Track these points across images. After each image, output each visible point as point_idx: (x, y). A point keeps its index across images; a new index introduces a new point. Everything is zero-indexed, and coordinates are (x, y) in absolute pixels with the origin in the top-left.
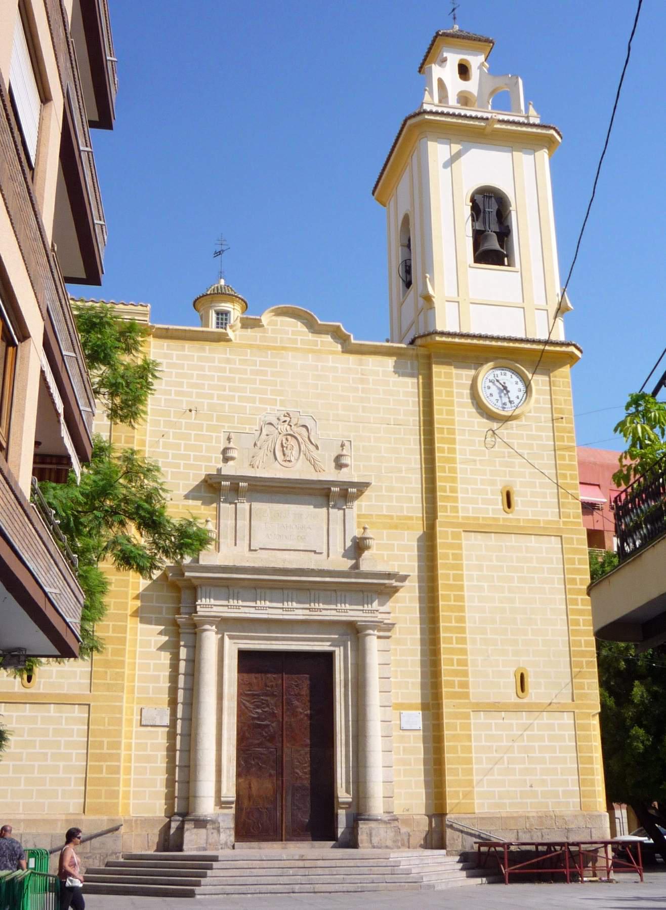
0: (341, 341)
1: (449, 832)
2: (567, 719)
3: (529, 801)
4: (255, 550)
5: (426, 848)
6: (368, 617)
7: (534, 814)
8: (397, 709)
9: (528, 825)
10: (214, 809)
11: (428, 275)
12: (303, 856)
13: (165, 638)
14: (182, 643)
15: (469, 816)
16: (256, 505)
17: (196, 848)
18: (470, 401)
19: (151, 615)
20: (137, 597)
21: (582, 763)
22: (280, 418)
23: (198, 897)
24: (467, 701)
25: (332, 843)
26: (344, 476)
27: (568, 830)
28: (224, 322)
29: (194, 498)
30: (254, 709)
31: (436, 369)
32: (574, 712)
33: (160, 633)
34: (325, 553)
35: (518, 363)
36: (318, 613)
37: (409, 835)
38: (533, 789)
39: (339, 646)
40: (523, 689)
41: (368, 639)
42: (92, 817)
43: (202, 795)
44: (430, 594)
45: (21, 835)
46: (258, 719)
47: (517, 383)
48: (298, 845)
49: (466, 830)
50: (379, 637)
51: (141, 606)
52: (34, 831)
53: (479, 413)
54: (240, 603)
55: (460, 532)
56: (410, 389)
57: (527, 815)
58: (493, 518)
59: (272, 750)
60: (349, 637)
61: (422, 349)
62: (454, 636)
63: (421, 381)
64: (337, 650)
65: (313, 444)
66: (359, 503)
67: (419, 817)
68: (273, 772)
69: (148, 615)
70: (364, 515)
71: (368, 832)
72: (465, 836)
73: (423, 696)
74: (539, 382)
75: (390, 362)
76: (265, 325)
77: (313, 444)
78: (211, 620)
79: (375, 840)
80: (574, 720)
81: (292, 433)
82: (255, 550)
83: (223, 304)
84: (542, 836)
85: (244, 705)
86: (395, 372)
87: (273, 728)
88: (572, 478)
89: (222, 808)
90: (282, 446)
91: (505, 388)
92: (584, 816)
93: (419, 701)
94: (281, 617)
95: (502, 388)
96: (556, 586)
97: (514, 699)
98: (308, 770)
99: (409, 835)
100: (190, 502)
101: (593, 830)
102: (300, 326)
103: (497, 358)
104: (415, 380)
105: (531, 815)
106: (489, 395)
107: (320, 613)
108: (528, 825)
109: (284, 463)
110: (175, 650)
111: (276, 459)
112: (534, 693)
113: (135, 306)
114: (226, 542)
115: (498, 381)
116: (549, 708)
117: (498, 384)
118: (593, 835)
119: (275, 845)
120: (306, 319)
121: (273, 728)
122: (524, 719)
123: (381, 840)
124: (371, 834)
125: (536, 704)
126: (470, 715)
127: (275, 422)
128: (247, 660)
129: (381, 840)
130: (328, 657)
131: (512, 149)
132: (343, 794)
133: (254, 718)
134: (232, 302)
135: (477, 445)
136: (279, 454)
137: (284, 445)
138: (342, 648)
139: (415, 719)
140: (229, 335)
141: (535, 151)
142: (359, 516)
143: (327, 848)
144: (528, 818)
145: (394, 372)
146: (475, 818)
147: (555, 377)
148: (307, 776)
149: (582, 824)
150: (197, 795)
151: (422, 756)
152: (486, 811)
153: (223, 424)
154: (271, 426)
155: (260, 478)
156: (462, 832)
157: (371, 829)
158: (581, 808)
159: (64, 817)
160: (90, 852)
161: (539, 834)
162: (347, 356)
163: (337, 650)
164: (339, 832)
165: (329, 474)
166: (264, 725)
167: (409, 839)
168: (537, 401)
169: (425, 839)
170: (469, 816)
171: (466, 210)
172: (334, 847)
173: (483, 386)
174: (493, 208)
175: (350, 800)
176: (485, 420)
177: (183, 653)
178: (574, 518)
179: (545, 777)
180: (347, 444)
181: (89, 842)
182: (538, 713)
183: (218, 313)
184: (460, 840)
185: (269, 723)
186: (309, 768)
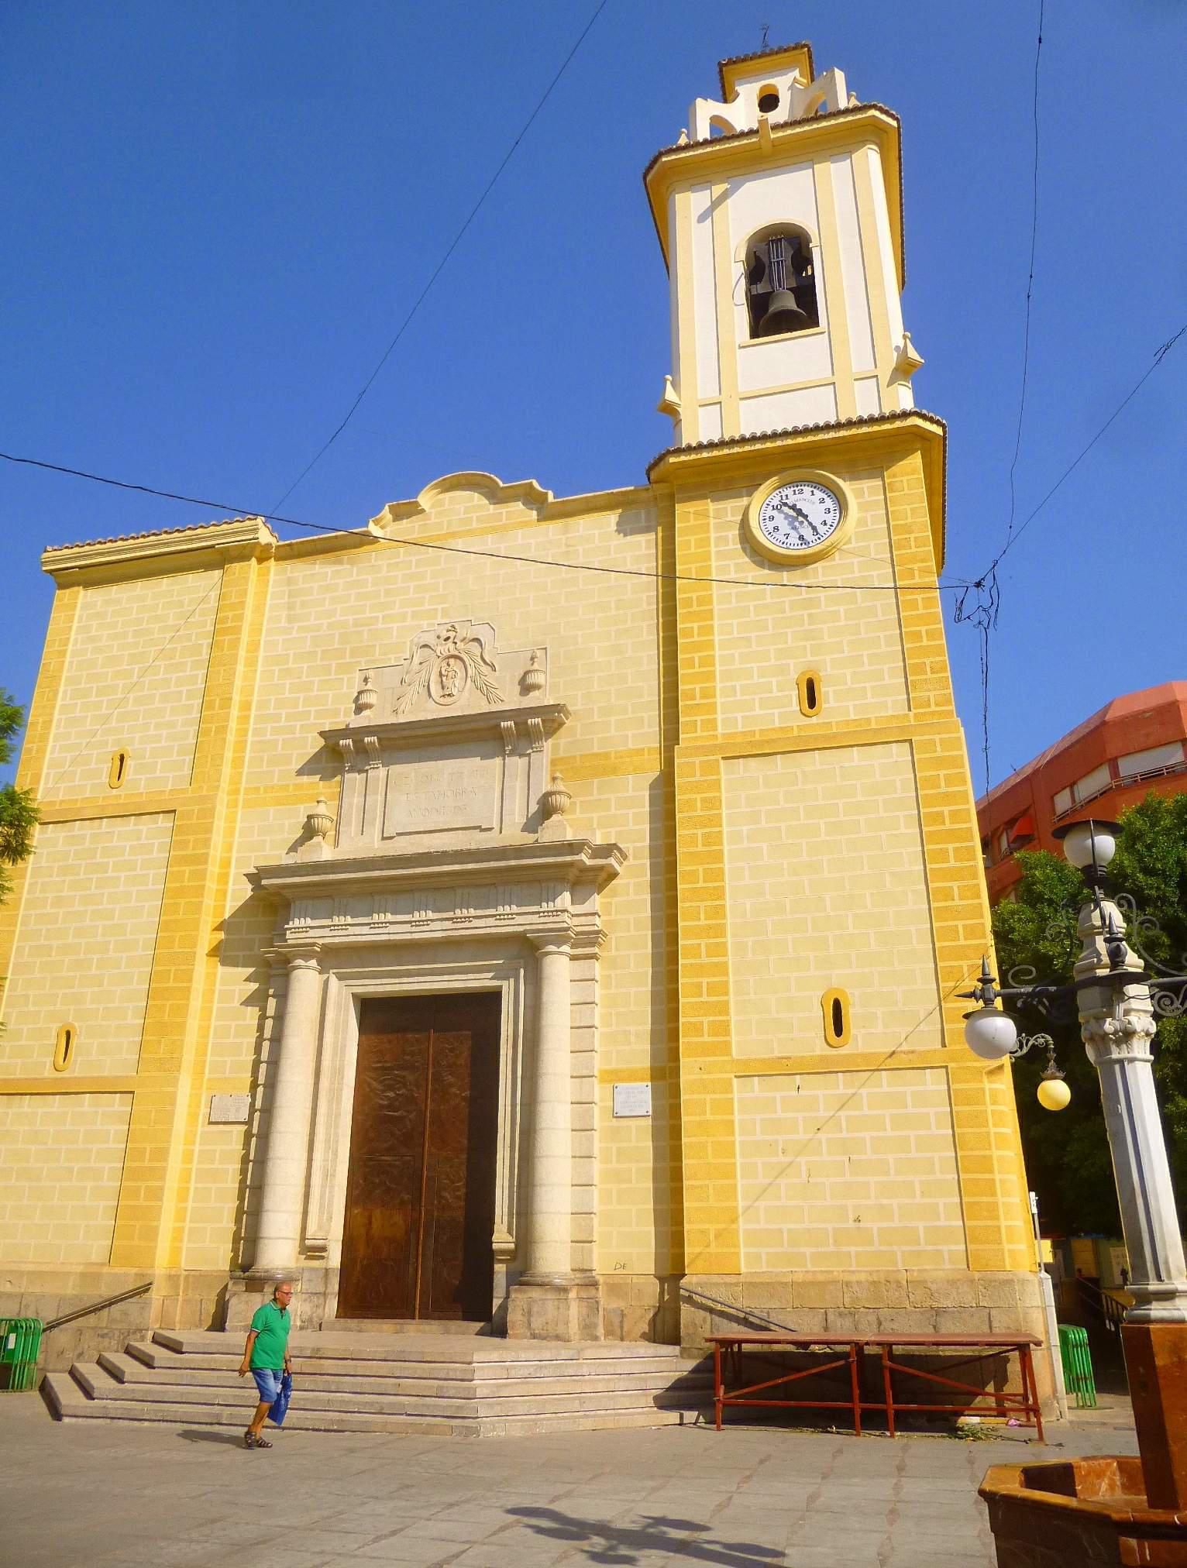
0: (538, 505)
1: (685, 1308)
2: (933, 1083)
3: (853, 1249)
4: (391, 838)
5: (654, 1342)
6: (550, 922)
7: (863, 1277)
8: (610, 1081)
9: (847, 1300)
10: (297, 1259)
11: (669, 377)
12: (318, 1349)
13: (254, 986)
14: (271, 991)
15: (728, 1279)
16: (396, 769)
17: (244, 1326)
18: (739, 546)
19: (237, 953)
20: (218, 928)
21: (967, 1171)
22: (441, 635)
23: (66, 1420)
24: (726, 1058)
25: (479, 1325)
26: (533, 700)
27: (938, 1312)
29: (311, 773)
30: (383, 1091)
31: (679, 508)
32: (946, 1067)
33: (248, 980)
34: (497, 829)
36: (467, 925)
37: (623, 1315)
38: (861, 1224)
39: (507, 979)
40: (839, 1030)
41: (548, 960)
42: (117, 1270)
43: (272, 1235)
44: (668, 876)
45: (22, 1295)
46: (390, 1107)
47: (822, 501)
48: (422, 1327)
49: (719, 1307)
50: (573, 958)
51: (226, 939)
52: (37, 1290)
53: (754, 562)
54: (349, 920)
55: (717, 761)
56: (644, 551)
57: (847, 1278)
58: (781, 728)
59: (408, 1158)
60: (522, 961)
61: (661, 485)
62: (703, 942)
63: (660, 535)
64: (507, 988)
65: (488, 664)
66: (556, 742)
67: (642, 1279)
68: (406, 1197)
69: (232, 954)
70: (562, 759)
71: (525, 1306)
72: (717, 1319)
73: (654, 1056)
74: (859, 492)
75: (612, 518)
77: (488, 664)
78: (306, 951)
79: (537, 1323)
80: (948, 1084)
81: (456, 653)
82: (391, 838)
84: (880, 1324)
85: (369, 1085)
86: (618, 531)
87: (410, 1120)
88: (931, 635)
89: (309, 1258)
90: (441, 675)
91: (799, 512)
92: (972, 1281)
93: (647, 1064)
94: (408, 937)
95: (795, 514)
96: (903, 830)
97: (820, 1049)
98: (461, 1192)
99: (623, 1315)
100: (305, 779)
101: (994, 1312)
102: (476, 498)
103: (784, 470)
104: (652, 536)
105: (854, 1278)
106: (771, 530)
107: (467, 925)
108: (847, 1300)
109: (442, 701)
110: (261, 1004)
111: (430, 695)
113: (170, 533)
114: (350, 830)
115: (785, 504)
116: (891, 1062)
117: (785, 509)
118: (995, 1324)
119: (385, 1327)
120: (487, 487)
121: (410, 1120)
122: (840, 1085)
123: (547, 1323)
124: (529, 1313)
125: (866, 1057)
126: (731, 1085)
127: (432, 641)
128: (371, 1010)
129: (547, 1323)
130: (492, 998)
131: (811, 162)
132: (502, 1238)
133: (382, 1107)
135: (752, 614)
136: (435, 689)
137: (443, 672)
138: (512, 981)
139: (641, 1097)
141: (851, 152)
142: (554, 763)
143: (470, 1334)
144: (848, 1284)
145: (616, 531)
146: (736, 1284)
147: (894, 476)
148: (462, 1203)
149: (969, 1300)
150: (262, 1236)
151: (651, 1165)
152: (764, 1270)
153: (358, 659)
154: (426, 649)
155: (392, 724)
156: (711, 1311)
157: (531, 1302)
158: (968, 1267)
159: (80, 1269)
160: (106, 1328)
161: (872, 1318)
162: (545, 525)
163: (504, 984)
164: (494, 1304)
165: (511, 700)
166: (396, 1117)
167: (622, 1322)
168: (861, 522)
169: (653, 1322)
170: (728, 1279)
171: (737, 271)
172: (481, 1333)
173: (762, 518)
174: (787, 254)
175: (512, 1246)
176: (767, 571)
177: (272, 1003)
178: (937, 705)
179: (885, 1201)
180: (539, 653)
181: (107, 1309)
182: (869, 1073)
184: (708, 1326)
185: (405, 1114)
186: (464, 1190)
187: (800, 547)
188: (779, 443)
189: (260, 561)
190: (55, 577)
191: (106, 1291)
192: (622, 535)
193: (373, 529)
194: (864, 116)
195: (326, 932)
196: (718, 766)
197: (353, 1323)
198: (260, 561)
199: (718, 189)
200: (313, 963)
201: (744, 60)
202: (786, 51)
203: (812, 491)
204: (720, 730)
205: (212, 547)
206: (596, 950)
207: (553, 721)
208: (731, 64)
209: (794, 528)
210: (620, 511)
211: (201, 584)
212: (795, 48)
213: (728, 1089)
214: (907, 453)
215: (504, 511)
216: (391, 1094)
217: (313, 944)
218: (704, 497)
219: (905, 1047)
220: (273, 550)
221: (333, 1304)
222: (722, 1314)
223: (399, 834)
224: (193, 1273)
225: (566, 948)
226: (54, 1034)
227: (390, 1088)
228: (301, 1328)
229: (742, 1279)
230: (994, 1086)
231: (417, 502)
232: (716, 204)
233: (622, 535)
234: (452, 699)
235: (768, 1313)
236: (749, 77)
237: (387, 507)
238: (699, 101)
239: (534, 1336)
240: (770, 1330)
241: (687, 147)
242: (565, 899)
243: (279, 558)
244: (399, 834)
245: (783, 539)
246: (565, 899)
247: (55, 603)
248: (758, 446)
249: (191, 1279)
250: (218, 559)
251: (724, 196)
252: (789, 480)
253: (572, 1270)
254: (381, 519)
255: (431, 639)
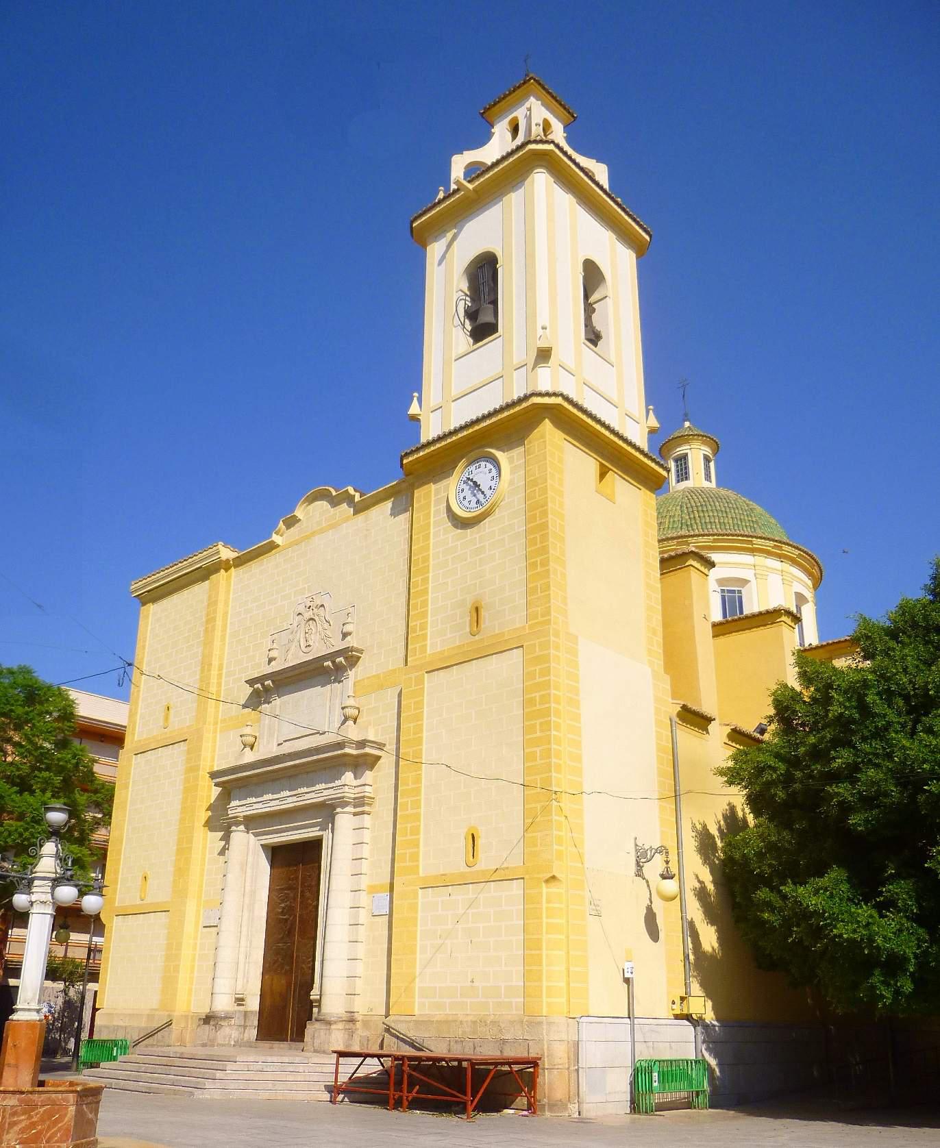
7: (470, 1018)
24: (415, 876)
27: (504, 1041)
28: (684, 471)
35: (492, 448)
36: (268, 805)
49: (401, 1036)
50: (355, 814)
56: (403, 527)
72: (401, 1043)
75: (388, 505)
76: (301, 518)
83: (678, 450)
91: (475, 483)
94: (278, 808)
97: (464, 869)
112: (486, 861)
134: (687, 442)
140: (275, 541)
156: (398, 1037)
159: (147, 1012)
161: (471, 1044)
168: (511, 483)
173: (457, 491)
176: (460, 531)
183: (676, 461)
188: (460, 435)
189: (226, 570)
190: (139, 599)
191: (156, 1025)
193: (276, 538)
194: (524, 151)
195: (244, 808)
196: (424, 677)
197: (267, 1044)
198: (226, 570)
199: (450, 235)
200: (242, 827)
204: (428, 652)
205: (200, 567)
206: (366, 808)
207: (352, 656)
209: (475, 495)
211: (199, 590)
213: (416, 897)
216: (283, 905)
217: (237, 817)
218: (428, 483)
219: (505, 865)
220: (231, 562)
221: (254, 1033)
222: (403, 1040)
223: (285, 741)
224: (195, 1014)
225: (349, 809)
226: (463, 838)
227: (283, 901)
228: (234, 1046)
229: (414, 1018)
230: (550, 890)
231: (294, 515)
232: (449, 246)
234: (311, 648)
235: (423, 1040)
237: (281, 522)
238: (532, 98)
239: (315, 1051)
240: (423, 1050)
241: (445, 198)
242: (348, 777)
243: (236, 566)
244: (285, 741)
245: (467, 505)
246: (348, 777)
247: (141, 615)
249: (194, 1018)
250: (204, 574)
252: (473, 459)
253: (346, 1012)
254: (279, 530)
255: (301, 609)
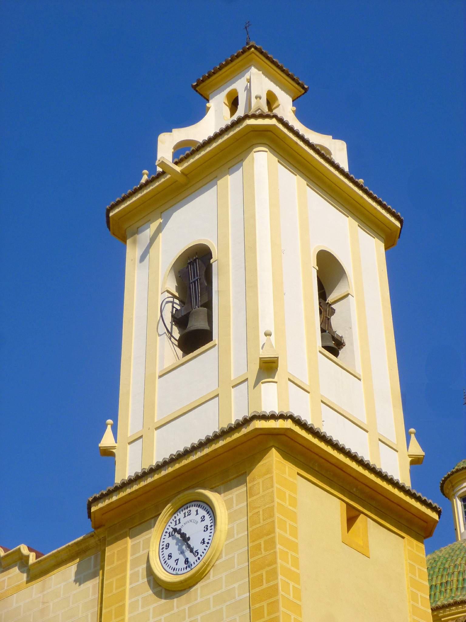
75: (71, 569)
86: (176, 528)
176: (163, 601)
187: (185, 571)
192: (78, 584)
201: (210, 76)
202: (237, 56)
203: (197, 511)
208: (200, 83)
210: (78, 560)
212: (243, 52)
214: (265, 451)
215: (6, 578)
233: (78, 584)
236: (217, 88)
248: (150, 480)
251: (159, 230)
